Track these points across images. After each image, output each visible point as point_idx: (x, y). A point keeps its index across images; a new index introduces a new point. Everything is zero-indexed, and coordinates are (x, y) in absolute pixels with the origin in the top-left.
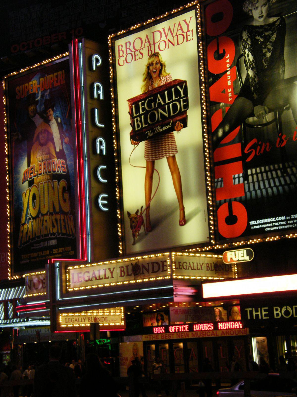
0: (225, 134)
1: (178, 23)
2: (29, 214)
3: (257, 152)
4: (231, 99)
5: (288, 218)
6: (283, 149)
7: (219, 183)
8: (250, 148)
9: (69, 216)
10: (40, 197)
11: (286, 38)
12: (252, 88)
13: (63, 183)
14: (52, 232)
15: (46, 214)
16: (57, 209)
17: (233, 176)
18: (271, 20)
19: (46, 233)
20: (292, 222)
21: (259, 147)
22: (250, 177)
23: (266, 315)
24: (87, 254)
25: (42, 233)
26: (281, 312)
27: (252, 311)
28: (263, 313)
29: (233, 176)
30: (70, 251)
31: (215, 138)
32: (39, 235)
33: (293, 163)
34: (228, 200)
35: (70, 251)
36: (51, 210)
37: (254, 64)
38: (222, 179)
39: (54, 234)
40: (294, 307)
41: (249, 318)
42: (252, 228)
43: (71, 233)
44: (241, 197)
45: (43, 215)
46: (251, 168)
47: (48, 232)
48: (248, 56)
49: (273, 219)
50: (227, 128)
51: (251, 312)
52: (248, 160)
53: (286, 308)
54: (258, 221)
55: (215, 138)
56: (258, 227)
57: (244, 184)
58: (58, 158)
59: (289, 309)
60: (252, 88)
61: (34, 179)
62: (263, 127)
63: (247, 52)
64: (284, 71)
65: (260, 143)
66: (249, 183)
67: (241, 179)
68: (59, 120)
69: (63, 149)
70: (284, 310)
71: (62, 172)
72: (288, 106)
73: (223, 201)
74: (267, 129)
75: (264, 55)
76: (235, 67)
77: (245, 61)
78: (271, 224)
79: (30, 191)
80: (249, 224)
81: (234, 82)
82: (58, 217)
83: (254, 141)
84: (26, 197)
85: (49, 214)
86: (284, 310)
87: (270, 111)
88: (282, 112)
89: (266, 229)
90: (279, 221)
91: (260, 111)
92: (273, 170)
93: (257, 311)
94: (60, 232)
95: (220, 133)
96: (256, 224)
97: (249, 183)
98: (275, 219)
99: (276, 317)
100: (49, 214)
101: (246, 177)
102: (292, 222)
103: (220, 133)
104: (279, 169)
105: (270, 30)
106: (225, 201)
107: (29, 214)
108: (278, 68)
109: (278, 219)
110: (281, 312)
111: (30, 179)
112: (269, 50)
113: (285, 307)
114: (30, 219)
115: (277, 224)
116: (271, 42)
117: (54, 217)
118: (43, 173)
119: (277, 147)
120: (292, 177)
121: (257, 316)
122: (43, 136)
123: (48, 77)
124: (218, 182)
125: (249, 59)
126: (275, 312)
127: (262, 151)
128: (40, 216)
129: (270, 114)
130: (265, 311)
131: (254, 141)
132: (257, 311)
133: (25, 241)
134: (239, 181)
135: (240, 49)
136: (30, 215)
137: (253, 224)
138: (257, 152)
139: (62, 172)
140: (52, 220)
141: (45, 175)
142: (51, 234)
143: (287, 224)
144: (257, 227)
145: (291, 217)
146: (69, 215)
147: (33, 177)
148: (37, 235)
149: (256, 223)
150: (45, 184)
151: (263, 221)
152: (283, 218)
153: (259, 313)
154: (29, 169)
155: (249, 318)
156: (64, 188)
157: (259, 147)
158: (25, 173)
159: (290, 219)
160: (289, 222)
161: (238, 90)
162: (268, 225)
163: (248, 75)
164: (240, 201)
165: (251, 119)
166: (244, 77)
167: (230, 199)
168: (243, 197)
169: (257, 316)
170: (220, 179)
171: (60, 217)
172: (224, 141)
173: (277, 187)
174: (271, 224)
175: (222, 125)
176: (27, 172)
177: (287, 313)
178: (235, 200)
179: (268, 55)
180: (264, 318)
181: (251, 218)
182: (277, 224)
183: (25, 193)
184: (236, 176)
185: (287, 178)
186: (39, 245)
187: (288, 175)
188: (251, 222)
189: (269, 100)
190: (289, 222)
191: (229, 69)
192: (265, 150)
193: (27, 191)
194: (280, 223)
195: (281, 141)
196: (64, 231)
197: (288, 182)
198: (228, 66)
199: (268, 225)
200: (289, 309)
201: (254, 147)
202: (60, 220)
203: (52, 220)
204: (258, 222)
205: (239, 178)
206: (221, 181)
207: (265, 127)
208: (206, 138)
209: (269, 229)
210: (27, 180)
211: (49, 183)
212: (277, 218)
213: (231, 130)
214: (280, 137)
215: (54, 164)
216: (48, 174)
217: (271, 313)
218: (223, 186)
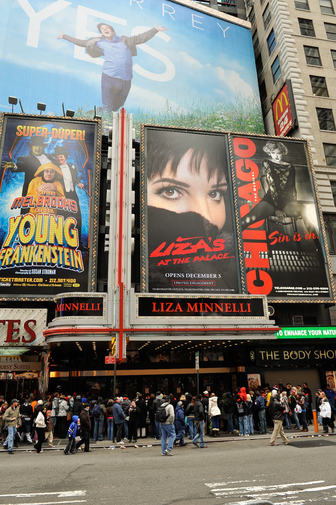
0: (252, 222)
1: (50, 254)
2: (17, 239)
3: (279, 240)
4: (257, 200)
5: (304, 289)
6: (298, 243)
7: (248, 255)
8: (274, 236)
9: (77, 251)
10: (36, 227)
11: (296, 177)
12: (273, 198)
13: (71, 221)
14: (49, 261)
15: (44, 244)
16: (60, 242)
17: (259, 252)
18: (285, 163)
19: (40, 261)
20: (307, 292)
21: (280, 238)
22: (274, 256)
23: (277, 357)
24: (330, 238)
25: (34, 261)
26: (289, 355)
27: (266, 353)
28: (275, 355)
29: (259, 252)
30: (73, 283)
31: (243, 223)
32: (30, 261)
33: (306, 253)
34: (255, 268)
35: (73, 283)
36: (52, 241)
37: (274, 184)
38: (250, 252)
39: (53, 264)
40: (299, 352)
41: (272, 359)
42: (276, 291)
43: (77, 267)
44: (266, 268)
45: (38, 244)
46: (275, 250)
47: (44, 261)
48: (269, 178)
49: (293, 288)
50: (254, 218)
51: (265, 354)
52: (272, 244)
53: (293, 352)
54: (281, 287)
55: (243, 223)
56: (281, 291)
57: (269, 260)
58: (67, 197)
59: (296, 353)
60: (273, 198)
61: (29, 209)
62: (283, 225)
63: (268, 175)
64: (296, 196)
65: (281, 235)
66: (272, 259)
67: (267, 256)
68: (73, 167)
69: (75, 191)
70: (291, 353)
71: (71, 210)
72: (300, 217)
73: (251, 268)
74: (286, 227)
75: (281, 181)
76: (259, 181)
77: (267, 180)
78: (292, 291)
79: (22, 218)
80: (273, 288)
81: (259, 191)
82: (60, 249)
83: (276, 232)
84: (15, 223)
85: (47, 244)
86: (291, 353)
87: (288, 216)
88: (297, 219)
89: (288, 294)
90: (298, 290)
91: (280, 214)
92: (288, 255)
93: (269, 353)
94: (61, 263)
95: (248, 220)
96: (280, 289)
97: (272, 259)
98: (295, 288)
99: (285, 359)
100: (47, 244)
101: (270, 255)
102: (307, 292)
103: (248, 220)
104: (296, 255)
105: (284, 168)
106: (253, 269)
107: (17, 239)
108: (292, 192)
109: (296, 288)
110: (289, 355)
111: (23, 207)
112: (285, 180)
113: (292, 352)
114: (18, 244)
115: (296, 292)
116: (285, 175)
117: (54, 248)
118: (45, 206)
119: (287, 241)
120: (310, 262)
121: (270, 357)
122: (49, 174)
123: (63, 130)
124: (246, 253)
125: (270, 180)
126: (285, 355)
127: (283, 240)
128: (34, 243)
129: (288, 218)
130: (276, 353)
131: (276, 232)
132: (269, 353)
133: (7, 264)
134: (265, 257)
135: (262, 172)
136: (18, 240)
137: (277, 289)
138: (279, 240)
139: (71, 210)
140: (51, 251)
141: (46, 208)
142: (48, 264)
143: (304, 293)
144: (280, 291)
145: (306, 289)
146: (76, 250)
147: (29, 206)
148: (26, 261)
149: (279, 289)
150: (45, 216)
151: (285, 288)
152: (301, 288)
153: (272, 355)
154: (24, 198)
155: (272, 359)
156: (72, 227)
157: (280, 238)
158: (17, 200)
159: (306, 290)
160: (305, 292)
161: (263, 196)
162: (289, 291)
163: (269, 189)
164: (266, 270)
165: (273, 218)
166: (267, 190)
167: (257, 268)
168: (268, 268)
169: (270, 357)
170: (248, 252)
171: (63, 249)
172: (250, 227)
173: (291, 267)
174: (292, 291)
175: (250, 215)
176: (20, 200)
177: (294, 356)
178: (262, 269)
179: (284, 182)
180: (275, 359)
181: (274, 285)
182: (296, 292)
183: (14, 218)
184: (262, 253)
185: (303, 262)
186: (28, 271)
187: (303, 260)
188: (275, 287)
189: (287, 208)
190: (305, 292)
191: (253, 181)
192: (285, 240)
193: (18, 218)
194: (298, 292)
195: (297, 237)
196: (67, 264)
197: (304, 265)
198: (254, 179)
199: (289, 291)
200: (296, 353)
201: (277, 236)
202: (63, 252)
203: (51, 251)
204: (281, 288)
205: (265, 254)
206: (249, 254)
207: (284, 226)
208: (18, 299)
209: (289, 294)
210: (19, 208)
211: (52, 216)
212: (296, 288)
213: (257, 220)
214: (296, 235)
215: (60, 202)
216: (50, 208)
217: (281, 356)
218: (251, 257)
